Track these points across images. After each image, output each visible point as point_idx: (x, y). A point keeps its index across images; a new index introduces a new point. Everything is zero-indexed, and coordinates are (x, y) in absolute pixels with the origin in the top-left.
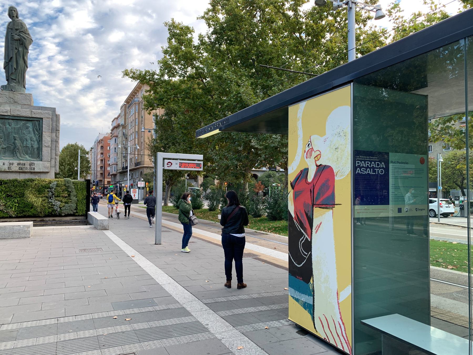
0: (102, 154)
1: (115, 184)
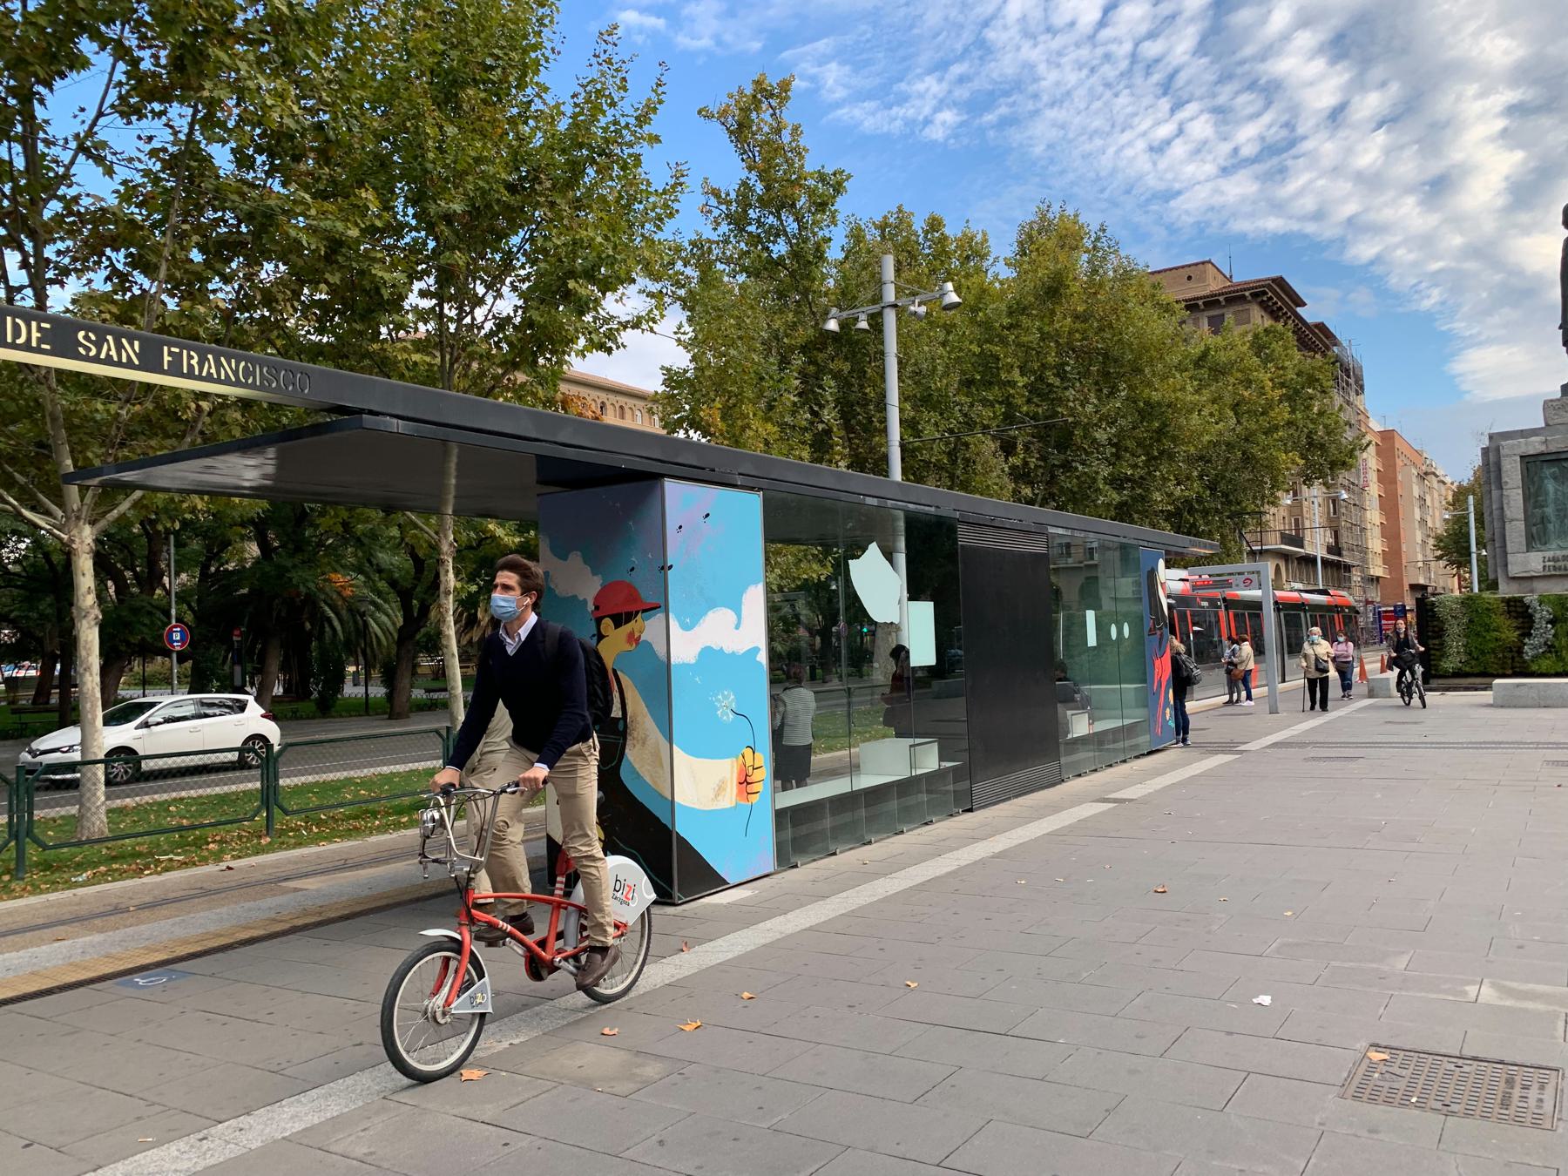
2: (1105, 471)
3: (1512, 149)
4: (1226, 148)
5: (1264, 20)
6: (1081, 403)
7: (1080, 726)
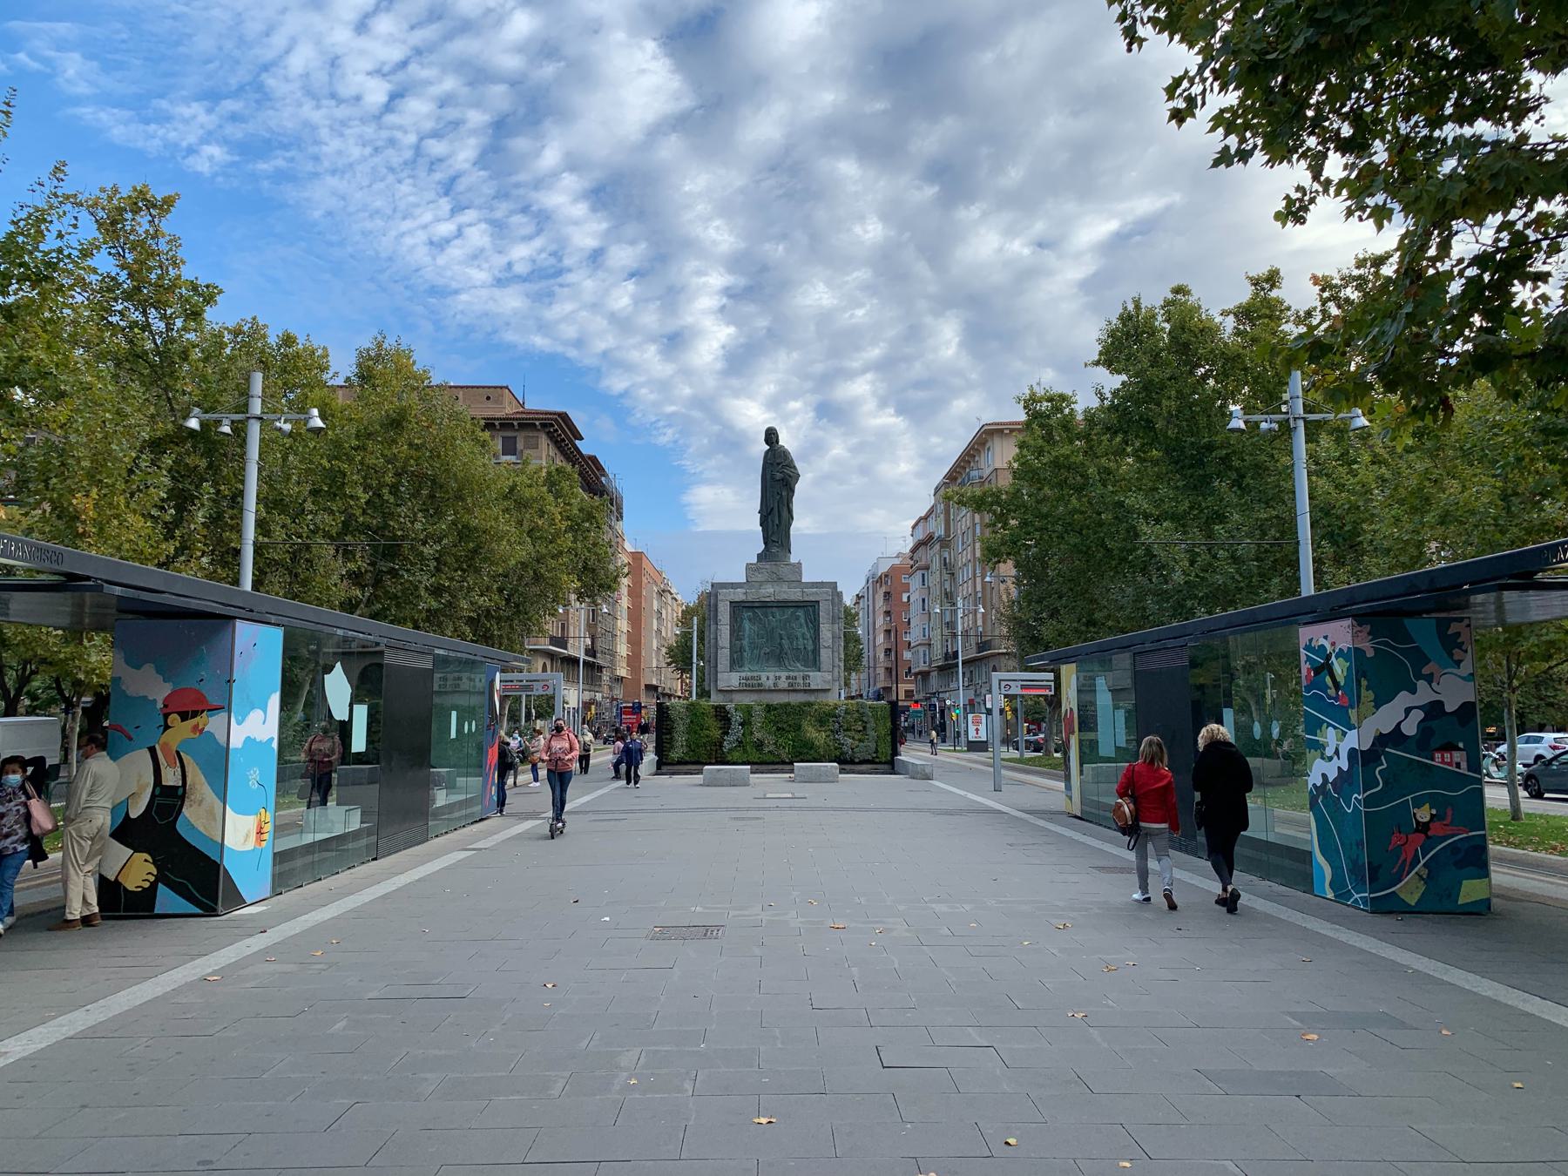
0: (888, 613)
1: (927, 699)
2: (427, 581)
3: (728, 324)
4: (501, 261)
5: (538, 153)
6: (410, 520)
7: (441, 798)
